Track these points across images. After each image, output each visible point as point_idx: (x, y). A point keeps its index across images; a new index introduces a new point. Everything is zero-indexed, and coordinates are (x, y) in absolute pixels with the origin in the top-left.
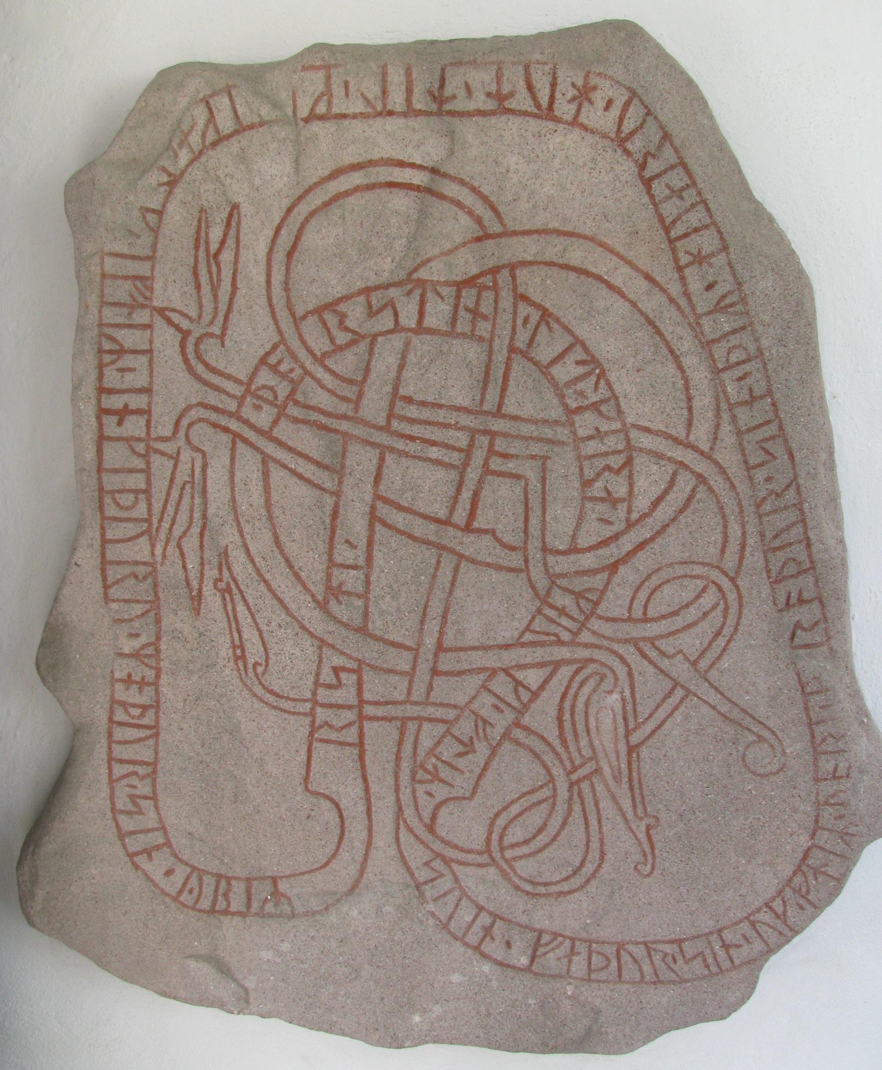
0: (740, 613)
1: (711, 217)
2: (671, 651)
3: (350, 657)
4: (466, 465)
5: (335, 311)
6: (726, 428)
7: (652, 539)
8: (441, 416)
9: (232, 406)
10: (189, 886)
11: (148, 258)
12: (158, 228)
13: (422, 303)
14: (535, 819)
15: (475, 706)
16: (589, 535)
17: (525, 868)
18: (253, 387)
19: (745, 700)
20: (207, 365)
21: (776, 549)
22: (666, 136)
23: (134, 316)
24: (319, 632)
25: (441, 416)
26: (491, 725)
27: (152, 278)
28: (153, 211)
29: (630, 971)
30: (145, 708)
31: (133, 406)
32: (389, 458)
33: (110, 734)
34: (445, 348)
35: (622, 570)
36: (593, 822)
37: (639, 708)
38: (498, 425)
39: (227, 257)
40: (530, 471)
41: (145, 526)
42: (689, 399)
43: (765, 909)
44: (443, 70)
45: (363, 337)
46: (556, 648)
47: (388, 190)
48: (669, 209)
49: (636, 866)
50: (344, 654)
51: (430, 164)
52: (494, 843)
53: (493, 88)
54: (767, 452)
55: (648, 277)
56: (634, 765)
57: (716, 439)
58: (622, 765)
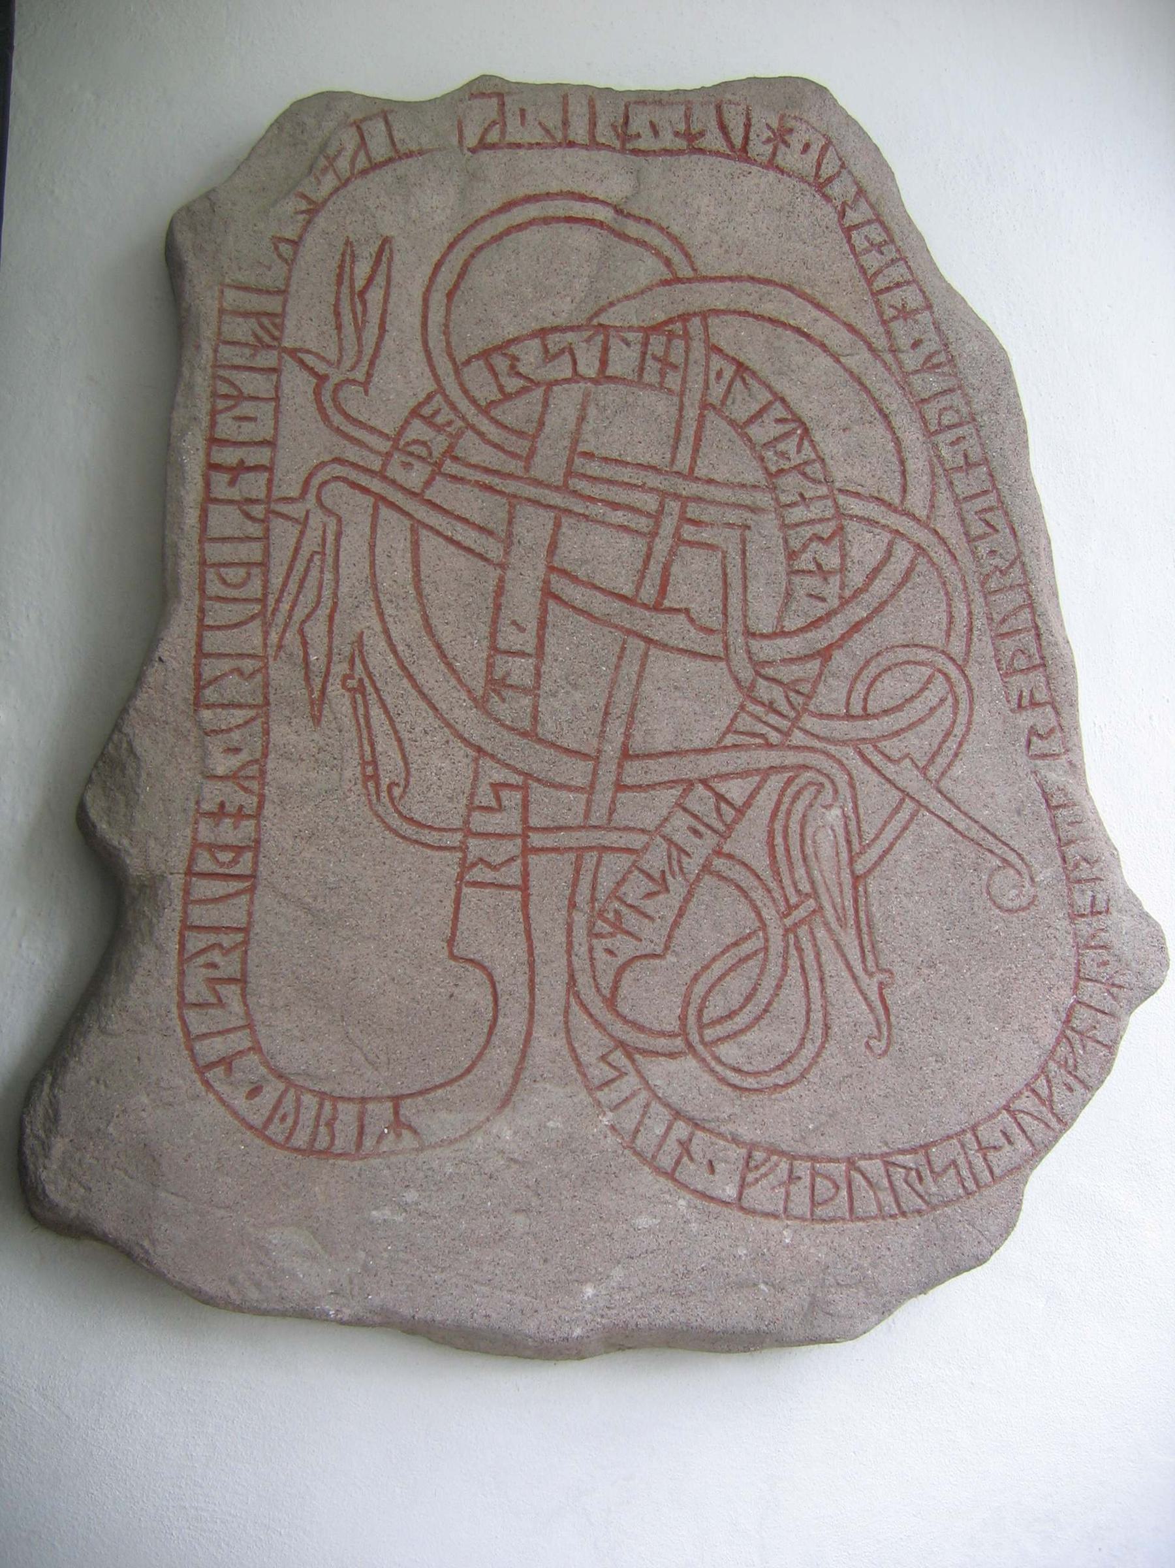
0: (971, 709)
1: (912, 274)
2: (896, 755)
3: (515, 770)
4: (654, 534)
5: (505, 355)
6: (944, 496)
7: (869, 619)
8: (625, 474)
9: (376, 465)
10: (281, 1112)
11: (279, 292)
12: (293, 260)
13: (605, 349)
14: (737, 985)
15: (667, 829)
16: (804, 610)
17: (728, 1052)
18: (402, 443)
19: (984, 815)
20: (347, 416)
21: (1003, 636)
22: (861, 192)
23: (258, 358)
24: (476, 739)
25: (625, 474)
26: (688, 855)
27: (283, 315)
28: (288, 241)
29: (866, 1202)
30: (239, 850)
31: (250, 462)
32: (566, 521)
33: (187, 891)
34: (631, 399)
35: (838, 656)
36: (815, 984)
37: (865, 827)
38: (694, 489)
39: (375, 296)
40: (729, 541)
41: (257, 608)
42: (902, 462)
43: (1027, 1094)
44: (627, 107)
45: (538, 384)
46: (763, 752)
47: (567, 225)
48: (872, 261)
49: (867, 1043)
50: (508, 766)
51: (615, 201)
52: (692, 1020)
53: (682, 127)
54: (988, 524)
55: (851, 328)
56: (862, 900)
57: (933, 506)
58: (847, 903)
